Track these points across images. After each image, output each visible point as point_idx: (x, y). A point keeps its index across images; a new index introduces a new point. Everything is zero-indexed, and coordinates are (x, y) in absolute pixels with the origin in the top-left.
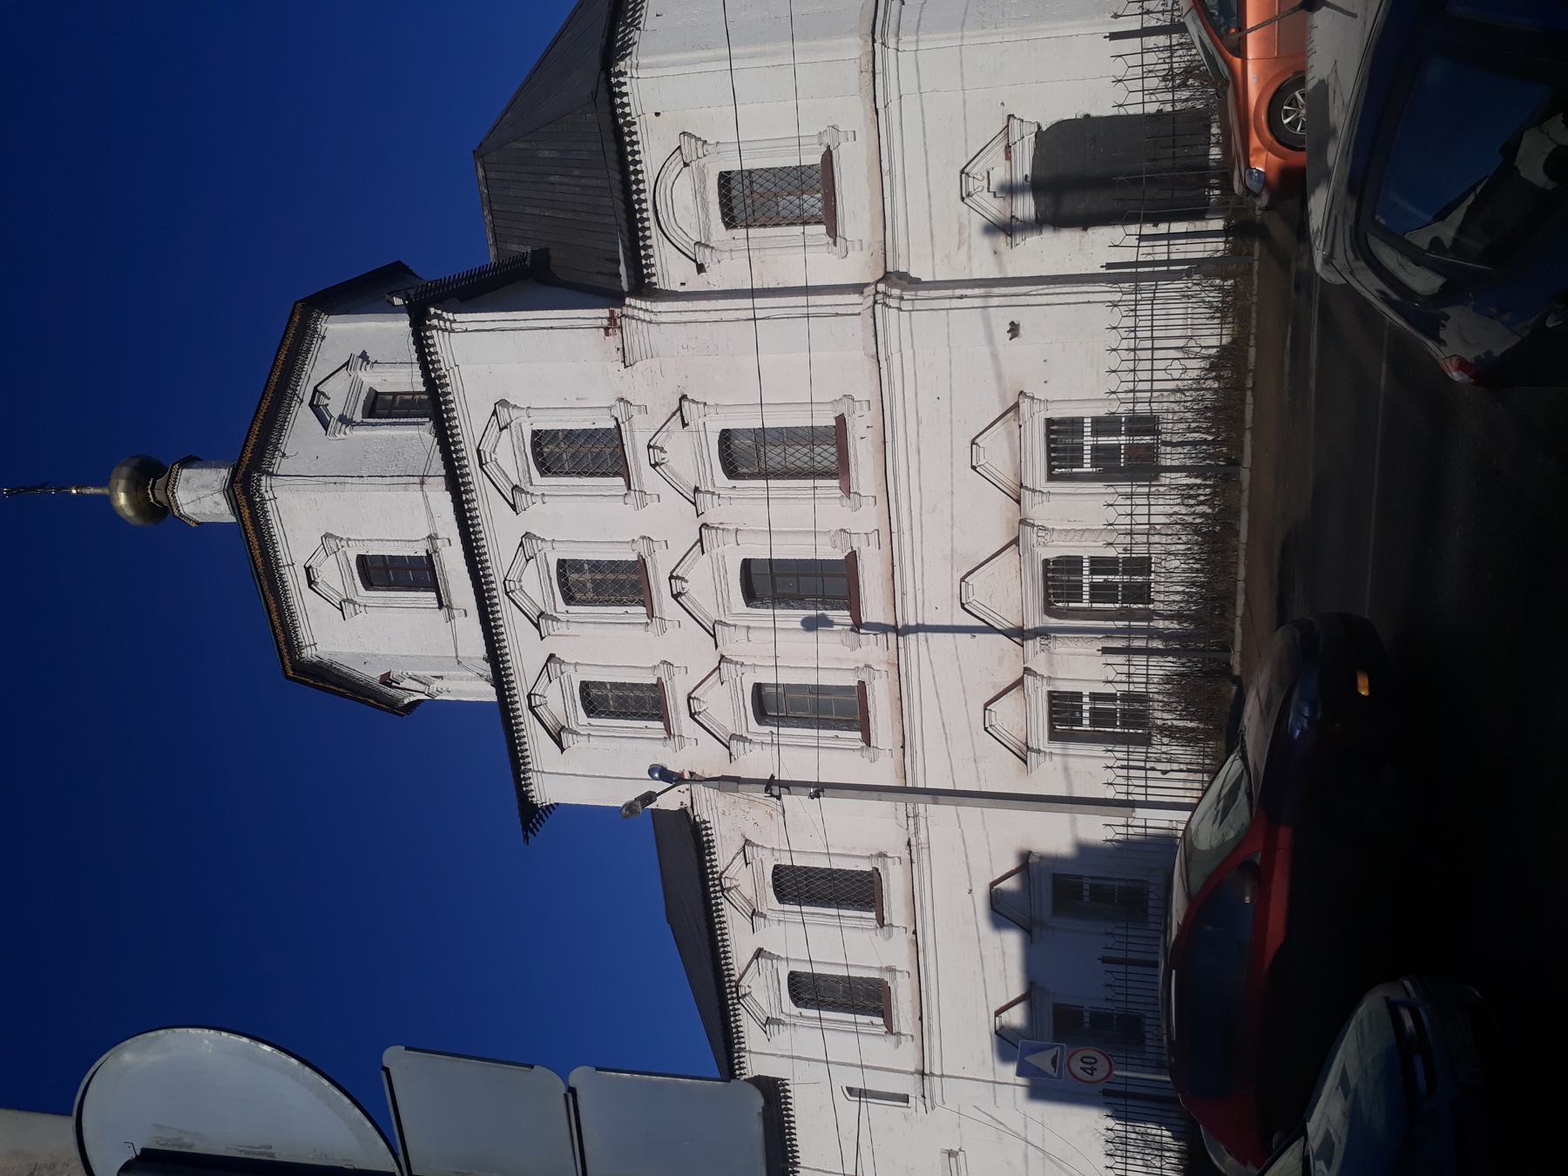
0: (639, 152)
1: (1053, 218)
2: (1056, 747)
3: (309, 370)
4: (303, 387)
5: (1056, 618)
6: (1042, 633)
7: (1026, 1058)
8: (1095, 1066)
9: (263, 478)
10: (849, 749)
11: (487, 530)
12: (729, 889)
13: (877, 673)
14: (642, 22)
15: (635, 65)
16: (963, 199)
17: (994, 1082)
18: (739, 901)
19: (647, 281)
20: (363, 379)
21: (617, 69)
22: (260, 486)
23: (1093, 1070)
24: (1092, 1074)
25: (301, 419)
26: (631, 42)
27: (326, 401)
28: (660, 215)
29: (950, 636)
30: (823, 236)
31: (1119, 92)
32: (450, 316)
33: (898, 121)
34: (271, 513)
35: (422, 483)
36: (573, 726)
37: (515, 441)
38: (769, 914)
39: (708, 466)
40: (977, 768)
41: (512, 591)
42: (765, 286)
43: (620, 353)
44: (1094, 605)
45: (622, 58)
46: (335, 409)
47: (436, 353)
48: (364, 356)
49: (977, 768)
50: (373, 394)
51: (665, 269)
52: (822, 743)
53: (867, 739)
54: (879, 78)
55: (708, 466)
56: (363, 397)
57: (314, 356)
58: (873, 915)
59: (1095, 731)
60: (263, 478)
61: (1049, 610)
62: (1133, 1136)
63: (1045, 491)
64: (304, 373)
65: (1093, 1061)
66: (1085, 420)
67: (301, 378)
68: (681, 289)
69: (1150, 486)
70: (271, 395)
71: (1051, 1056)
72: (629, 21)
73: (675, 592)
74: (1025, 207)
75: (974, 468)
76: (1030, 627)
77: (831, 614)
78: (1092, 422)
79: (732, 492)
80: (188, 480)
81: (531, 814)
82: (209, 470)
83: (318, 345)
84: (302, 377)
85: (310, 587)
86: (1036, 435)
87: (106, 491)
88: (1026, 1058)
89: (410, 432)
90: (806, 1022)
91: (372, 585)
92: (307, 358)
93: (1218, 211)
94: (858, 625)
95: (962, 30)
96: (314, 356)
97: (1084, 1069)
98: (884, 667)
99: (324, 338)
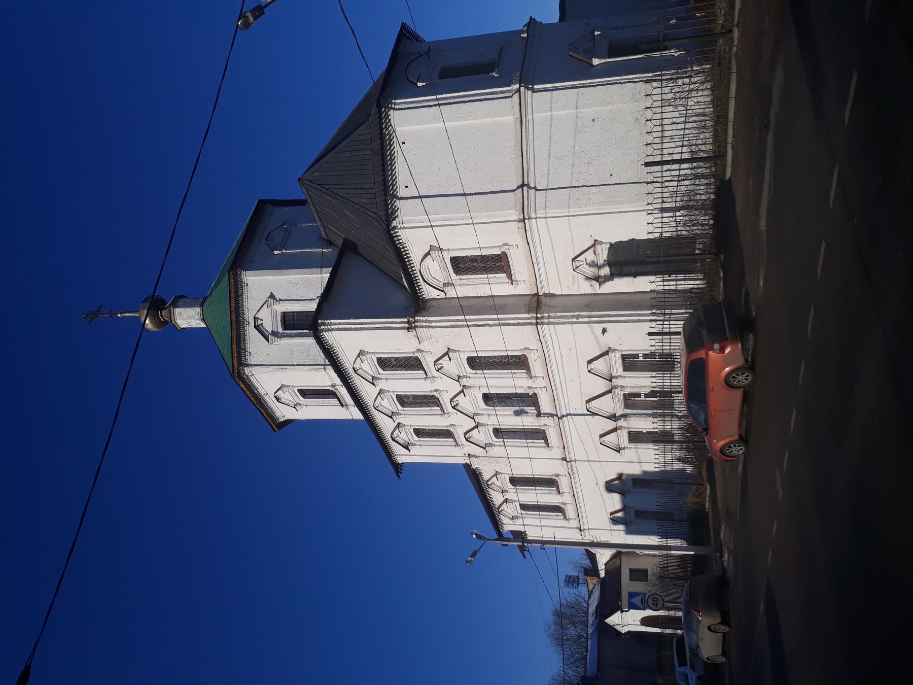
0: (409, 254)
1: (642, 624)
2: (632, 445)
3: (247, 305)
4: (247, 315)
5: (630, 409)
6: (625, 416)
7: (631, 600)
8: (657, 602)
9: (245, 368)
10: (539, 447)
11: (361, 388)
12: (491, 485)
13: (550, 427)
14: (398, 192)
15: (401, 222)
16: (574, 270)
17: (611, 530)
18: (496, 488)
19: (421, 297)
20: (276, 309)
21: (393, 225)
22: (244, 372)
23: (657, 604)
24: (656, 606)
25: (252, 337)
26: (396, 209)
27: (261, 322)
28: (424, 277)
29: (583, 416)
30: (505, 279)
31: (651, 228)
32: (329, 321)
33: (539, 243)
34: (252, 379)
35: (325, 369)
36: (413, 442)
37: (369, 362)
38: (509, 490)
39: (463, 368)
40: (598, 453)
41: (377, 407)
42: (479, 295)
43: (416, 337)
44: (647, 399)
45: (394, 219)
46: (268, 327)
47: (327, 339)
48: (272, 296)
49: (598, 453)
50: (283, 313)
51: (428, 292)
52: (529, 445)
53: (547, 443)
54: (528, 232)
55: (463, 368)
56: (279, 318)
57: (246, 297)
58: (555, 489)
59: (645, 361)
60: (245, 368)
61: (627, 406)
62: (667, 195)
63: (622, 375)
64: (244, 307)
65: (656, 600)
66: (640, 355)
67: (244, 310)
68: (438, 297)
69: (671, 374)
70: (235, 328)
71: (640, 599)
72: (392, 192)
73: (453, 406)
74: (606, 271)
75: (589, 371)
76: (619, 415)
77: (526, 409)
78: (643, 356)
79: (475, 375)
80: (180, 314)
81: (398, 468)
82: (189, 309)
83: (246, 290)
84: (245, 309)
85: (278, 402)
86: (618, 367)
87: (137, 315)
88: (631, 600)
89: (309, 341)
90: (529, 516)
91: (306, 394)
92: (243, 298)
93: (700, 272)
94: (539, 415)
95: (568, 209)
96: (246, 297)
97: (653, 604)
98: (553, 425)
99: (247, 284)
